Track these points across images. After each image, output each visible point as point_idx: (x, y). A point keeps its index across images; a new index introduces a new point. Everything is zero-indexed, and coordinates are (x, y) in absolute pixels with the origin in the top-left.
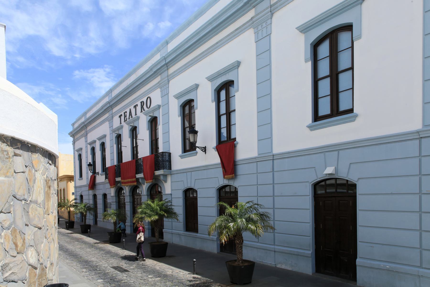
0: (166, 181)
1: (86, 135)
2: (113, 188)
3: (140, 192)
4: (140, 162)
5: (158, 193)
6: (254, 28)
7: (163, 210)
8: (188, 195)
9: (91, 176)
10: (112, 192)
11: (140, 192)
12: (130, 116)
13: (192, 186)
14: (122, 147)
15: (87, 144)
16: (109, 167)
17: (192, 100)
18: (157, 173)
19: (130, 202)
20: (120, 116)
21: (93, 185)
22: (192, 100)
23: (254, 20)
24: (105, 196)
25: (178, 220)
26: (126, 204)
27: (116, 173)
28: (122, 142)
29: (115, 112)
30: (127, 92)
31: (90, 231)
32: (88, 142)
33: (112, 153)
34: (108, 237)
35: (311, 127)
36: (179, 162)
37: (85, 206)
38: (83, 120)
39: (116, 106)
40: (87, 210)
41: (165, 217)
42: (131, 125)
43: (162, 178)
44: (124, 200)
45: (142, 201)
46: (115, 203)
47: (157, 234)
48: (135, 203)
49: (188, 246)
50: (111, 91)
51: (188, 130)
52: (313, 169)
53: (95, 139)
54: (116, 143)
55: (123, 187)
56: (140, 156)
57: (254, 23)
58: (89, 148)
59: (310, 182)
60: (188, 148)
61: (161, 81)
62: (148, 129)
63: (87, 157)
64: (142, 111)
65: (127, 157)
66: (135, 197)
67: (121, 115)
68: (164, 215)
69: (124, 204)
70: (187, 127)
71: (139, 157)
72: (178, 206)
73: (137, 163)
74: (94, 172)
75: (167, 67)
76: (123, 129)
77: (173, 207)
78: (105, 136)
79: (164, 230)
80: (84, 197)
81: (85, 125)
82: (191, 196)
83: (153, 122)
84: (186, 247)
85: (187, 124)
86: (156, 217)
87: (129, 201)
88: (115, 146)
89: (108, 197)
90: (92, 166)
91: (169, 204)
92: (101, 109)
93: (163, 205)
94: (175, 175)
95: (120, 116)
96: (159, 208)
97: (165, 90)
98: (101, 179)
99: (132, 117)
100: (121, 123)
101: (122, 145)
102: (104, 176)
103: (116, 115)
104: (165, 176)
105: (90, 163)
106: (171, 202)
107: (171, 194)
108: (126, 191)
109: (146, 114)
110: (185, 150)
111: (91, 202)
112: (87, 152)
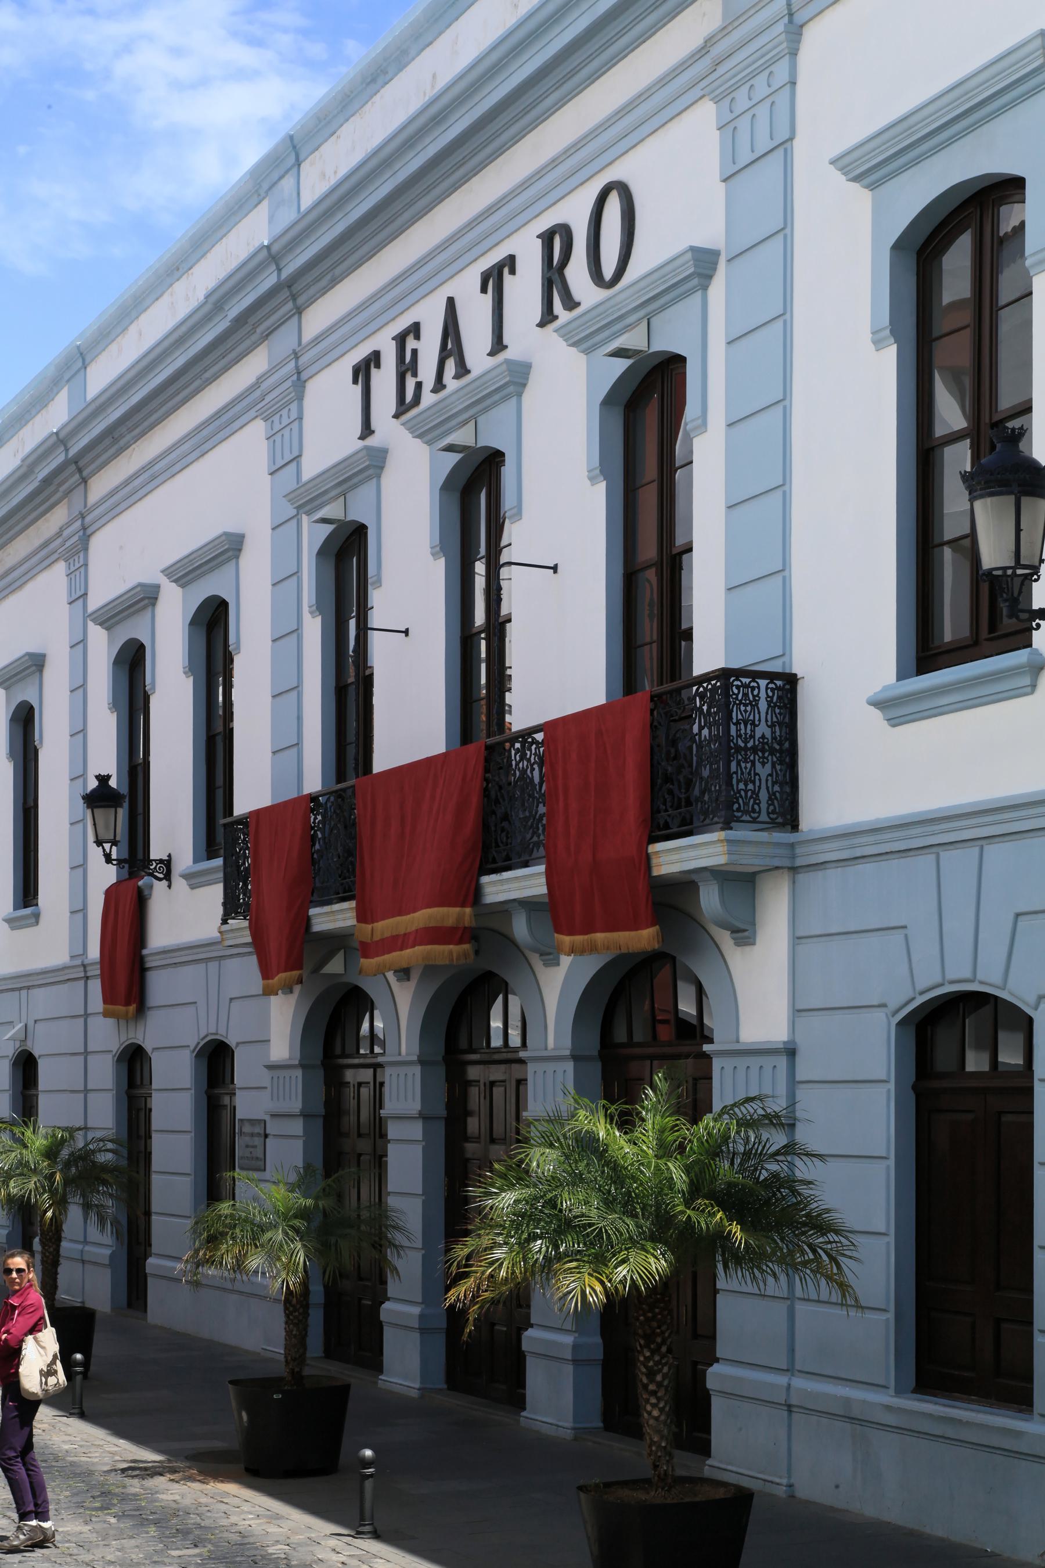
0: (744, 934)
1: (76, 548)
2: (288, 989)
3: (515, 1040)
4: (524, 764)
5: (666, 1033)
6: (266, 420)
7: (712, 1196)
8: (943, 1059)
9: (111, 895)
10: (274, 1030)
11: (515, 1040)
12: (450, 366)
13: (988, 979)
14: (377, 643)
15: (87, 617)
16: (257, 813)
17: (1011, 187)
18: (672, 857)
19: (425, 1117)
20: (363, 372)
21: (125, 967)
22: (1011, 187)
23: (718, 50)
24: (216, 1060)
25: (844, 1287)
26: (393, 1131)
27: (299, 866)
28: (376, 598)
29: (317, 340)
30: (431, 151)
31: (86, 1363)
32: (96, 601)
33: (286, 692)
34: (232, 1423)
35: (894, 708)
36: (873, 758)
37: (51, 1153)
38: (57, 415)
39: (335, 282)
40: (67, 1182)
41: (736, 1258)
42: (452, 439)
43: (710, 900)
44: (378, 1101)
45: (535, 1107)
46: (297, 1127)
47: (654, 1412)
48: (473, 1125)
49: (938, 1530)
50: (292, 153)
51: (958, 459)
52: (898, 937)
53: (147, 570)
54: (319, 607)
55: (372, 987)
56: (528, 706)
57: (268, 399)
58: (102, 649)
59: (893, 1005)
60: (952, 625)
61: (724, 30)
62: (604, 470)
63: (80, 733)
64: (548, 317)
65: (412, 721)
66: (473, 1072)
67: (374, 359)
68: (720, 1238)
69: (378, 1130)
70: (955, 438)
71: (518, 720)
72: (855, 1160)
73: (496, 781)
74: (136, 861)
75: (80, 471)
76: (530, 397)
77: (803, 1170)
78: (229, 549)
79: (151, 1261)
80: (47, 1075)
81: (75, 461)
82: (975, 1062)
83: (649, 403)
84: (912, 1533)
85: (950, 414)
86: (656, 1263)
87: (415, 1106)
88: (314, 630)
89: (245, 1070)
90: (120, 802)
91: (778, 1139)
92: (208, 318)
93: (716, 1148)
94: (833, 874)
95: (363, 372)
96: (687, 1169)
97: (762, 112)
98: (188, 913)
99: (463, 370)
100: (367, 430)
101: (377, 618)
102: (216, 893)
103: (327, 359)
104: (741, 883)
105: (103, 780)
106: (785, 1122)
107: (790, 1052)
108: (398, 1018)
109: (583, 341)
110: (926, 649)
111: (103, 1116)
112: (80, 688)
